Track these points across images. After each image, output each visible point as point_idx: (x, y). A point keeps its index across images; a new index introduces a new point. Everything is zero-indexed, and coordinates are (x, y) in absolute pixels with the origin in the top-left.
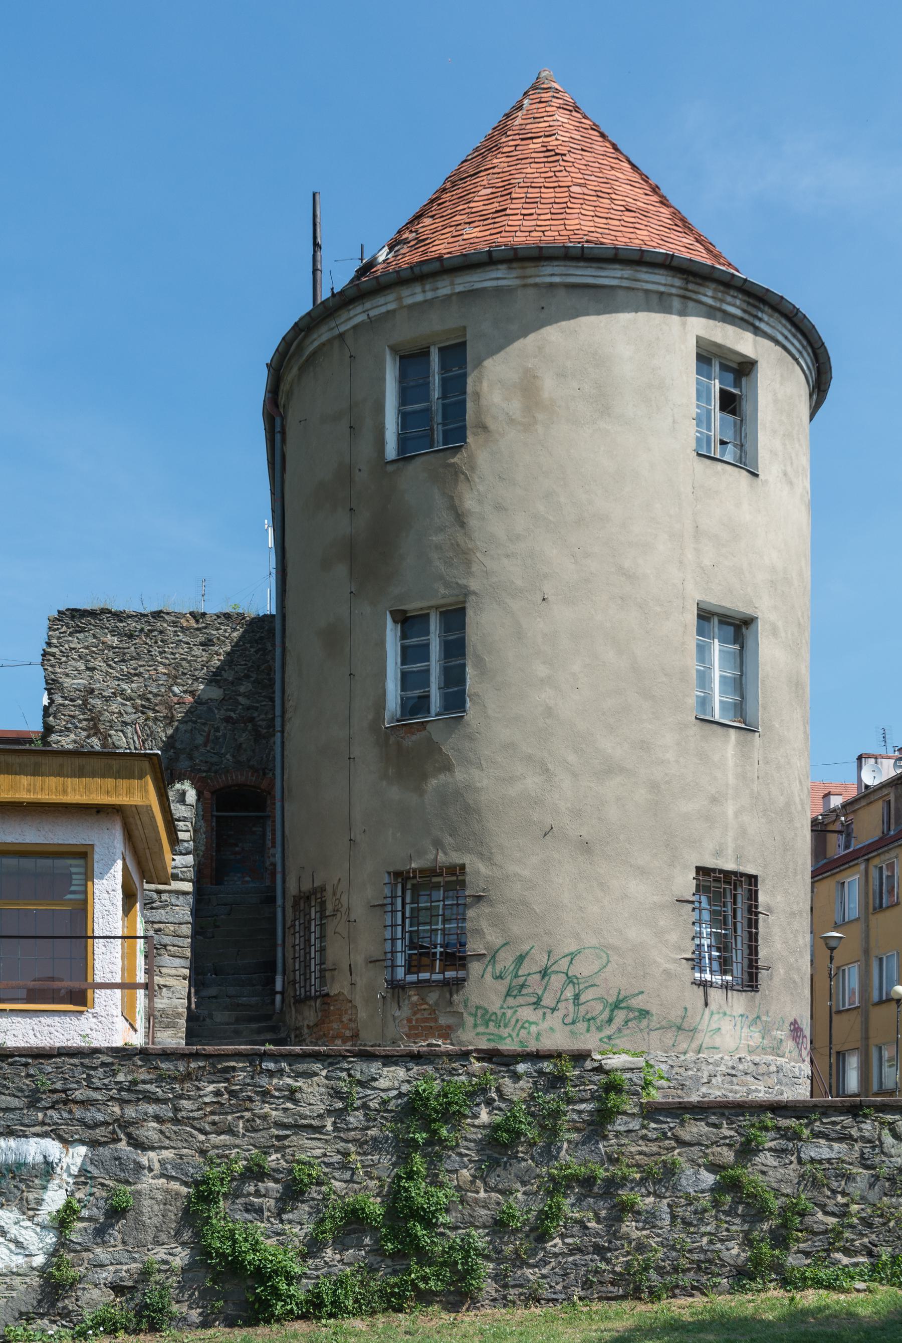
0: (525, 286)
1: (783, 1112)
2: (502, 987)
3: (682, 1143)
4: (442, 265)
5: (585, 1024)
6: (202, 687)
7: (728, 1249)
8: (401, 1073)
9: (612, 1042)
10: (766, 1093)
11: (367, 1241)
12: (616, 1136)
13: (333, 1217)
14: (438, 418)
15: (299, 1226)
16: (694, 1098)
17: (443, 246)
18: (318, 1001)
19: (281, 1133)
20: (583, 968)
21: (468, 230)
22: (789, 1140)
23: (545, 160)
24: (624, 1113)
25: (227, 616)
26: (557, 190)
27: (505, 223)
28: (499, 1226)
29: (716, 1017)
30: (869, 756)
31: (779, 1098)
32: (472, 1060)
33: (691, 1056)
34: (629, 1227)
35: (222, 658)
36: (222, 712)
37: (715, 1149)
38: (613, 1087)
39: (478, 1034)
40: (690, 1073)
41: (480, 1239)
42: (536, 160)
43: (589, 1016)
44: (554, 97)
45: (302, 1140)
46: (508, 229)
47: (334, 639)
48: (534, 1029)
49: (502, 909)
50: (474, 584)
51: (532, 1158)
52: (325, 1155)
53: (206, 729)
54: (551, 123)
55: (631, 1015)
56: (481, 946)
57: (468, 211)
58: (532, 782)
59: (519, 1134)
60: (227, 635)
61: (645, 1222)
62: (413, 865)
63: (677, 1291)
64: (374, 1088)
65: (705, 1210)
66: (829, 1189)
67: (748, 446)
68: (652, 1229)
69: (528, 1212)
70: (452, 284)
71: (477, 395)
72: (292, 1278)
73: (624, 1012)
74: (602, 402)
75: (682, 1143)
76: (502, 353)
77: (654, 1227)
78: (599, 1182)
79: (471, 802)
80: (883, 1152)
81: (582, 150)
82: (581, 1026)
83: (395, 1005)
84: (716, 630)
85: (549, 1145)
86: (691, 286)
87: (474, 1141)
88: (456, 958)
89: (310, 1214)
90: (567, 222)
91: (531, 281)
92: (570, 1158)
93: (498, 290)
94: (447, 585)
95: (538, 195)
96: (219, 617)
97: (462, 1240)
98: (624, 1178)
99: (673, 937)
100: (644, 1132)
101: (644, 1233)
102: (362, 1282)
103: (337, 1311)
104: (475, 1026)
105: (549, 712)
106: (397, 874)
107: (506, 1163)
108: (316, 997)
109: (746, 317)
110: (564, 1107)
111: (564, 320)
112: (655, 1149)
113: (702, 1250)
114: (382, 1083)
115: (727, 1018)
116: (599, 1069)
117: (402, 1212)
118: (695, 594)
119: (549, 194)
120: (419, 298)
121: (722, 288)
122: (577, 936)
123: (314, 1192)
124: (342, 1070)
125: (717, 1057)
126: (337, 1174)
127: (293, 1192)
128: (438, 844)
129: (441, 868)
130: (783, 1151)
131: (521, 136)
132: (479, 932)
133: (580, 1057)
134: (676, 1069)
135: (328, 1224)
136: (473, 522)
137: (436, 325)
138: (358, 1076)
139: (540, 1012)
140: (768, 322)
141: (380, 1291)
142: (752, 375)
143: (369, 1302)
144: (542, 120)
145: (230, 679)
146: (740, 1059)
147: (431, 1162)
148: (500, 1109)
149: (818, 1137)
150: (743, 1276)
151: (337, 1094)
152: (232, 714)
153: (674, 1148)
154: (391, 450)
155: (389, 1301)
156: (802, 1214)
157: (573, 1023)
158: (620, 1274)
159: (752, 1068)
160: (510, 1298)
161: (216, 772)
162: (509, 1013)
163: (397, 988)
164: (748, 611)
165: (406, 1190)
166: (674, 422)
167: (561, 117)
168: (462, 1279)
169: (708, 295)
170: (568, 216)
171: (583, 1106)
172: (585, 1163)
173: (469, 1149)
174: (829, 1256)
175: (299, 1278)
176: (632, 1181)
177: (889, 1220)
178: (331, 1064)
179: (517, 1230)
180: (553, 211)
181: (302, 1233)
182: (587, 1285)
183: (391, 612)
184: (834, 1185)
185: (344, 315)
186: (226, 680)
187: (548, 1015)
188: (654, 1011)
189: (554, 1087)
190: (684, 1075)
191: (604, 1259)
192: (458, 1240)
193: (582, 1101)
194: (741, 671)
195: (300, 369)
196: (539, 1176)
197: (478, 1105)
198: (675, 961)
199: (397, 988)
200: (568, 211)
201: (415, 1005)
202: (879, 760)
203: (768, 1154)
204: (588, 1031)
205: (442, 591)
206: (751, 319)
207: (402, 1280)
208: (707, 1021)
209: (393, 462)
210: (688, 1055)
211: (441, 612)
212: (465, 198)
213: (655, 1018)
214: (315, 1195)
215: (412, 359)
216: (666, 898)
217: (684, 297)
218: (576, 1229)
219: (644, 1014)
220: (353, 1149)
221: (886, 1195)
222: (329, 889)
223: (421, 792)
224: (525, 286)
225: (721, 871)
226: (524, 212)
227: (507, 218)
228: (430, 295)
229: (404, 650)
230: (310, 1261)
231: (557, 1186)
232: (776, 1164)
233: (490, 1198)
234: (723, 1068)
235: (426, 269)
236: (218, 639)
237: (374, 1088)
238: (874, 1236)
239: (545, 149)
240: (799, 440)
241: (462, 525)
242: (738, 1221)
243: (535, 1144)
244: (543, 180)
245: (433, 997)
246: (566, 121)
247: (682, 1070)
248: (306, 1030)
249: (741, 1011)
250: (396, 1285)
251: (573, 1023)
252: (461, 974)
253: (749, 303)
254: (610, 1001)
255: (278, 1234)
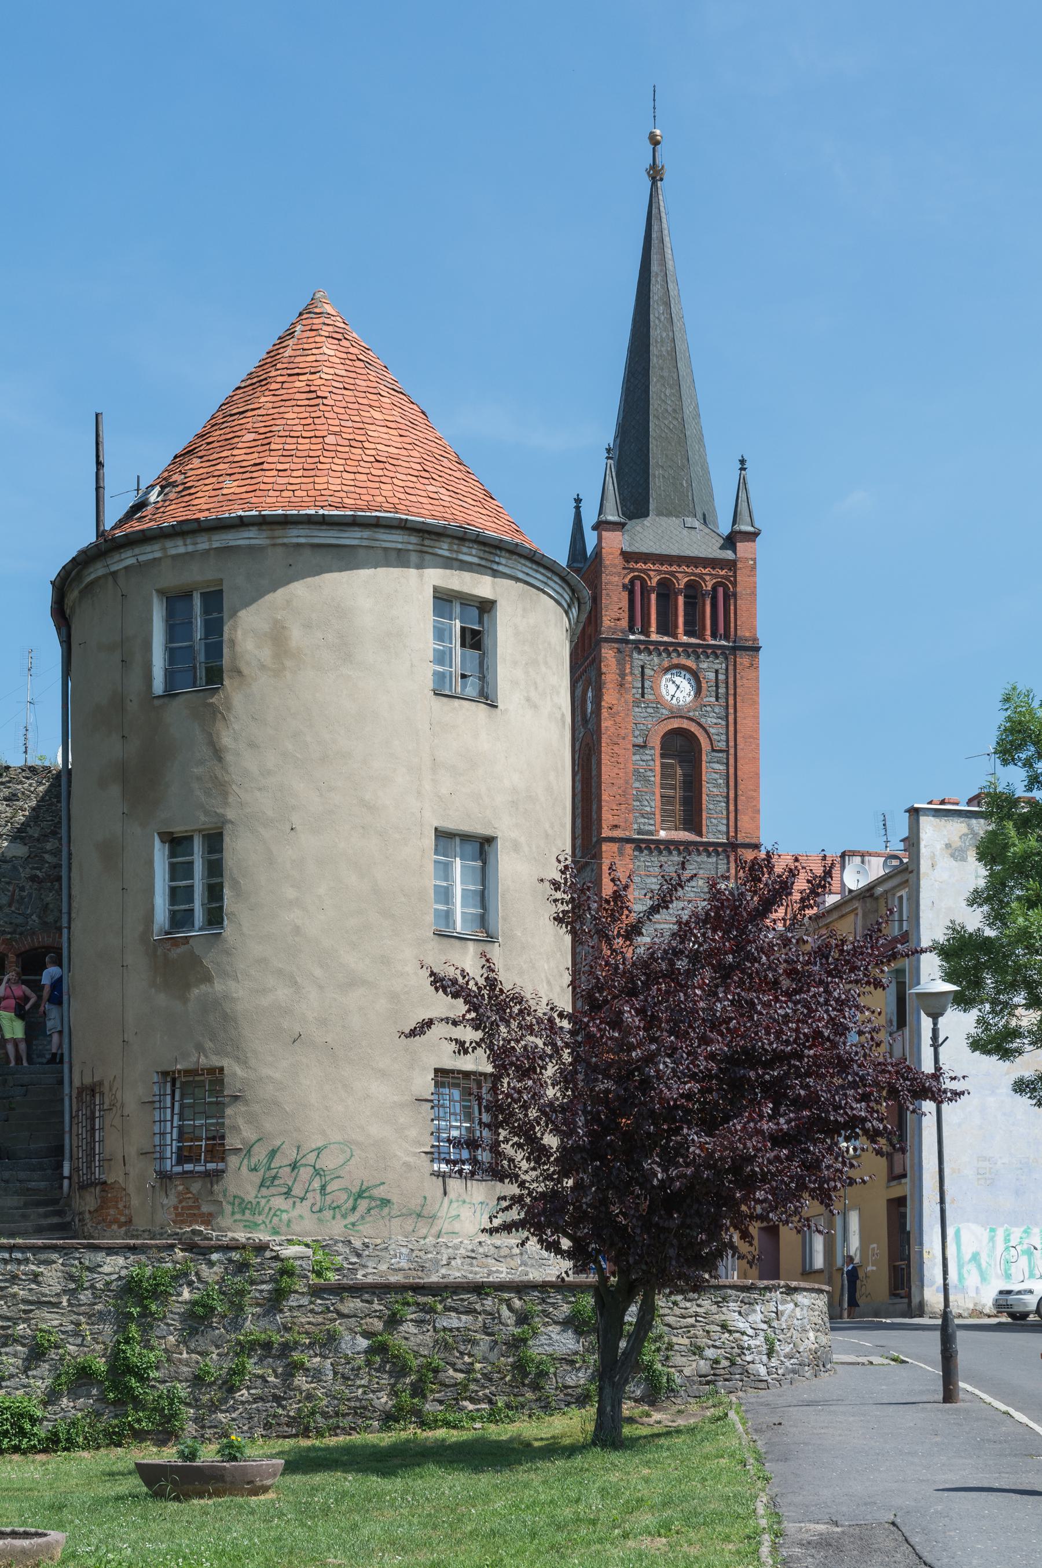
0: (274, 545)
1: (422, 1292)
2: (256, 1178)
3: (341, 1315)
4: (199, 525)
5: (331, 1212)
6: (6, 844)
7: (378, 1399)
8: (121, 1261)
9: (356, 1228)
10: (508, 1273)
11: (94, 1392)
12: (290, 1310)
13: (67, 1373)
14: (201, 657)
15: (41, 1381)
16: (434, 1278)
17: (204, 506)
18: (98, 1188)
19: (27, 1308)
20: (328, 1162)
21: (228, 483)
22: (427, 1313)
23: (307, 402)
24: (296, 1292)
25: (33, 770)
26: (314, 440)
27: (260, 480)
28: (198, 1380)
29: (455, 1205)
30: (854, 853)
31: (525, 1278)
32: (177, 1250)
33: (430, 1240)
34: (301, 1381)
35: (27, 813)
36: (28, 870)
37: (369, 1320)
38: (287, 1272)
39: (235, 1221)
40: (430, 1256)
41: (182, 1390)
42: (299, 403)
43: (335, 1205)
44: (324, 324)
45: (44, 1313)
46: (263, 486)
47: (111, 854)
48: (285, 1216)
49: (256, 1108)
50: (230, 814)
51: (224, 1327)
52: (61, 1325)
53: (11, 889)
54: (318, 358)
55: (373, 1204)
56: (238, 1141)
57: (231, 459)
58: (282, 994)
59: (213, 1309)
60: (32, 789)
61: (313, 1377)
62: (179, 1067)
63: (338, 1431)
64: (100, 1273)
65: (359, 1368)
66: (458, 1351)
67: (489, 678)
68: (319, 1382)
69: (221, 1369)
70: (210, 540)
71: (233, 642)
72: (36, 1420)
73: (367, 1201)
74: (345, 650)
75: (341, 1315)
76: (254, 606)
77: (320, 1381)
78: (276, 1345)
79: (228, 1011)
80: (501, 1323)
81: (345, 388)
82: (328, 1214)
83: (163, 1194)
84: (458, 849)
85: (237, 1317)
86: (427, 542)
87: (178, 1314)
88: (217, 1150)
89: (50, 1370)
90: (317, 480)
91: (280, 541)
92: (252, 1327)
93: (251, 548)
94: (206, 813)
95: (294, 447)
96: (23, 770)
97: (168, 1391)
98: (296, 1343)
99: (413, 1133)
100: (312, 1306)
101: (313, 1385)
102: (90, 1424)
103: (70, 1445)
104: (233, 1213)
105: (297, 930)
106: (165, 1074)
107: (203, 1331)
108: (97, 1184)
109: (483, 563)
110: (248, 1287)
111: (310, 576)
112: (320, 1320)
113: (357, 1399)
114: (106, 1269)
115: (467, 1206)
116: (276, 1258)
117: (121, 1369)
118: (434, 820)
119: (304, 445)
120: (182, 550)
121: (456, 542)
122: (323, 1133)
123: (53, 1354)
124: (75, 1259)
125: (457, 1241)
126: (71, 1340)
127: (36, 1354)
128: (200, 1048)
129: (202, 1070)
130: (422, 1321)
131: (289, 372)
132: (236, 1128)
133: (261, 1248)
134: (416, 1253)
135: (63, 1379)
136: (229, 758)
137: (196, 575)
138: (87, 1263)
139: (290, 1201)
140: (504, 563)
141: (104, 1430)
142: (493, 613)
143: (96, 1439)
144: (310, 352)
145: (36, 835)
146: (480, 1243)
147: (145, 1331)
148: (199, 1289)
149: (449, 1311)
150: (390, 1419)
151: (71, 1278)
152: (38, 873)
153: (335, 1320)
154: (158, 685)
155: (111, 1438)
156: (436, 1371)
157: (320, 1211)
158: (294, 1418)
159: (493, 1250)
160: (207, 1436)
161: (21, 934)
162: (263, 1201)
163: (164, 1177)
164: (488, 832)
165: (124, 1352)
166: (412, 666)
167: (329, 349)
168: (169, 1422)
169: (444, 549)
170: (319, 473)
171: (264, 1287)
172: (265, 1331)
173: (174, 1320)
174: (458, 1403)
175: (41, 1420)
176: (302, 1345)
177: (505, 1376)
178: (66, 1254)
179: (213, 1383)
180: (306, 466)
181: (44, 1386)
182: (267, 1426)
183: (159, 834)
184: (462, 1348)
185: (117, 557)
186: (31, 837)
187: (298, 1204)
188: (394, 1200)
189: (241, 1272)
190: (424, 1257)
191: (280, 1405)
192: (165, 1391)
193: (263, 1282)
194: (483, 882)
195: (80, 592)
196: (229, 1341)
197: (181, 1286)
198: (415, 1154)
199: (164, 1177)
200: (320, 466)
201: (179, 1194)
202: (867, 858)
203: (410, 1324)
204: (334, 1218)
205: (203, 818)
206: (488, 564)
207: (121, 1421)
208: (446, 1209)
209: (159, 697)
210: (427, 1240)
211: (204, 836)
212: (229, 443)
213: (395, 1206)
214: (53, 1356)
215: (177, 601)
216: (406, 1097)
217: (421, 552)
218: (259, 1381)
219: (386, 1202)
220: (83, 1320)
221: (503, 1356)
222: (106, 1084)
223: (185, 1000)
224: (274, 545)
225: (459, 1072)
226: (280, 467)
227: (262, 473)
228: (190, 548)
229: (173, 867)
230: (50, 1408)
231: (246, 1348)
232: (416, 1331)
233: (191, 1358)
234: (462, 1251)
235: (185, 528)
236: (23, 793)
237: (100, 1273)
238: (493, 1388)
239: (307, 389)
240: (546, 663)
241: (220, 759)
242: (386, 1376)
243: (226, 1316)
244: (300, 428)
245: (196, 1187)
246: (332, 353)
247: (421, 1254)
248: (87, 1216)
249: (480, 1199)
250: (117, 1426)
251: (320, 1211)
252: (221, 1166)
253: (485, 551)
254: (354, 1191)
255: (25, 1387)
